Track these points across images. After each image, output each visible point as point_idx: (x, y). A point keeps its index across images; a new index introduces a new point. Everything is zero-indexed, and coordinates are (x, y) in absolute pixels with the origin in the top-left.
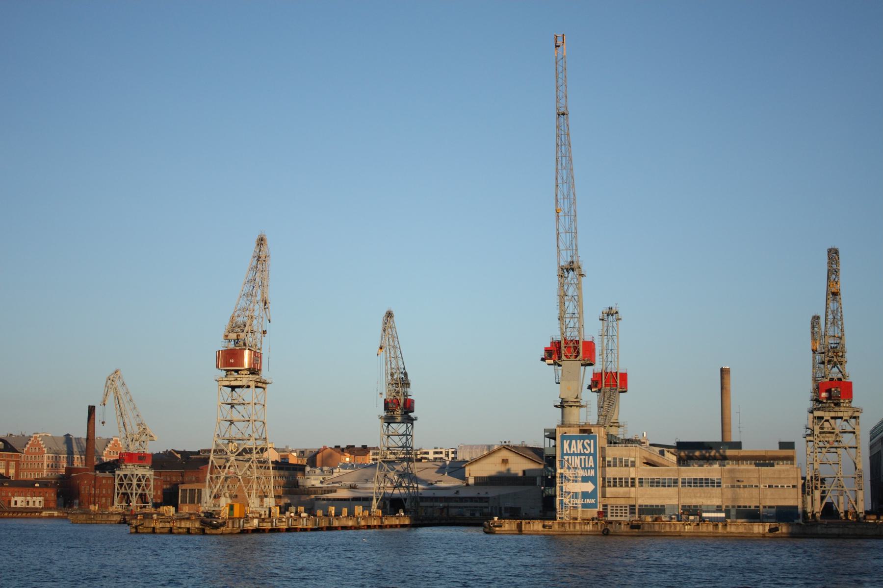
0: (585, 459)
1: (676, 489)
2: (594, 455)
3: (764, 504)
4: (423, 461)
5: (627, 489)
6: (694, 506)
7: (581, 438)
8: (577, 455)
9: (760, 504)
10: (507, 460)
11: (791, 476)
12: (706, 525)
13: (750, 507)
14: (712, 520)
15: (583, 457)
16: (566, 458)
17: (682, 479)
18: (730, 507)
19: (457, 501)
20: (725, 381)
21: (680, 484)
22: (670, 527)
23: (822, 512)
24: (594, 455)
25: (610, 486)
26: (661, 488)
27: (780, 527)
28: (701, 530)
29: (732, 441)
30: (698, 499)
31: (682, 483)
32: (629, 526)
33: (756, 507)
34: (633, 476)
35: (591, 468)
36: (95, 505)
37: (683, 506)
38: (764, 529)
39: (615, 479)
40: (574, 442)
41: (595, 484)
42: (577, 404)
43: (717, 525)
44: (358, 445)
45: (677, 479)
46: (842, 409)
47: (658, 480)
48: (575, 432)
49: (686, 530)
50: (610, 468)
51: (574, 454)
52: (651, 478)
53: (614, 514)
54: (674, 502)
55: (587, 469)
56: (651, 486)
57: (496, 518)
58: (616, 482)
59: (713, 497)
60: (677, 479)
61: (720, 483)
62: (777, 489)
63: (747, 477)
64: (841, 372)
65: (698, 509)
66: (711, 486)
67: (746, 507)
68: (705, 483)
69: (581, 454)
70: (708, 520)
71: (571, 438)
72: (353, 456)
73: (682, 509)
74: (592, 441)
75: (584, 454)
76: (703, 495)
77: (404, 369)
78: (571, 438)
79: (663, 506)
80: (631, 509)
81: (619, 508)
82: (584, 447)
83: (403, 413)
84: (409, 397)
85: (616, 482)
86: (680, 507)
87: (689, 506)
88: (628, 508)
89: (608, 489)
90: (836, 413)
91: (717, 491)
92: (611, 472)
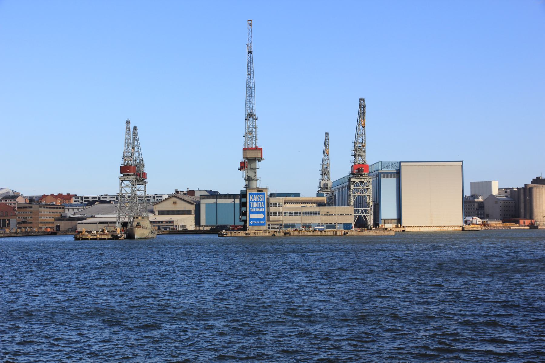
0: (260, 204)
1: (300, 216)
2: (264, 202)
3: (338, 223)
4: (112, 202)
5: (279, 216)
6: (308, 224)
7: (258, 194)
8: (256, 202)
10: (176, 202)
14: (319, 230)
15: (259, 203)
16: (251, 203)
17: (303, 212)
19: (156, 223)
20: (399, 186)
23: (374, 224)
24: (264, 202)
25: (271, 215)
30: (310, 221)
32: (284, 233)
33: (334, 224)
34: (281, 211)
35: (263, 208)
39: (274, 212)
40: (255, 196)
41: (264, 214)
42: (255, 179)
43: (322, 232)
44: (65, 193)
46: (364, 178)
48: (255, 191)
51: (255, 202)
53: (273, 228)
54: (300, 222)
55: (261, 208)
56: (289, 215)
57: (224, 231)
58: (275, 214)
62: (343, 216)
67: (330, 224)
69: (258, 201)
71: (253, 194)
72: (62, 200)
74: (263, 196)
75: (260, 201)
77: (142, 157)
78: (253, 194)
79: (294, 224)
80: (280, 226)
81: (275, 225)
82: (259, 198)
83: (324, 198)
84: (144, 172)
85: (275, 214)
86: (302, 224)
87: (306, 224)
88: (279, 225)
89: (271, 217)
91: (318, 217)
92: (272, 209)
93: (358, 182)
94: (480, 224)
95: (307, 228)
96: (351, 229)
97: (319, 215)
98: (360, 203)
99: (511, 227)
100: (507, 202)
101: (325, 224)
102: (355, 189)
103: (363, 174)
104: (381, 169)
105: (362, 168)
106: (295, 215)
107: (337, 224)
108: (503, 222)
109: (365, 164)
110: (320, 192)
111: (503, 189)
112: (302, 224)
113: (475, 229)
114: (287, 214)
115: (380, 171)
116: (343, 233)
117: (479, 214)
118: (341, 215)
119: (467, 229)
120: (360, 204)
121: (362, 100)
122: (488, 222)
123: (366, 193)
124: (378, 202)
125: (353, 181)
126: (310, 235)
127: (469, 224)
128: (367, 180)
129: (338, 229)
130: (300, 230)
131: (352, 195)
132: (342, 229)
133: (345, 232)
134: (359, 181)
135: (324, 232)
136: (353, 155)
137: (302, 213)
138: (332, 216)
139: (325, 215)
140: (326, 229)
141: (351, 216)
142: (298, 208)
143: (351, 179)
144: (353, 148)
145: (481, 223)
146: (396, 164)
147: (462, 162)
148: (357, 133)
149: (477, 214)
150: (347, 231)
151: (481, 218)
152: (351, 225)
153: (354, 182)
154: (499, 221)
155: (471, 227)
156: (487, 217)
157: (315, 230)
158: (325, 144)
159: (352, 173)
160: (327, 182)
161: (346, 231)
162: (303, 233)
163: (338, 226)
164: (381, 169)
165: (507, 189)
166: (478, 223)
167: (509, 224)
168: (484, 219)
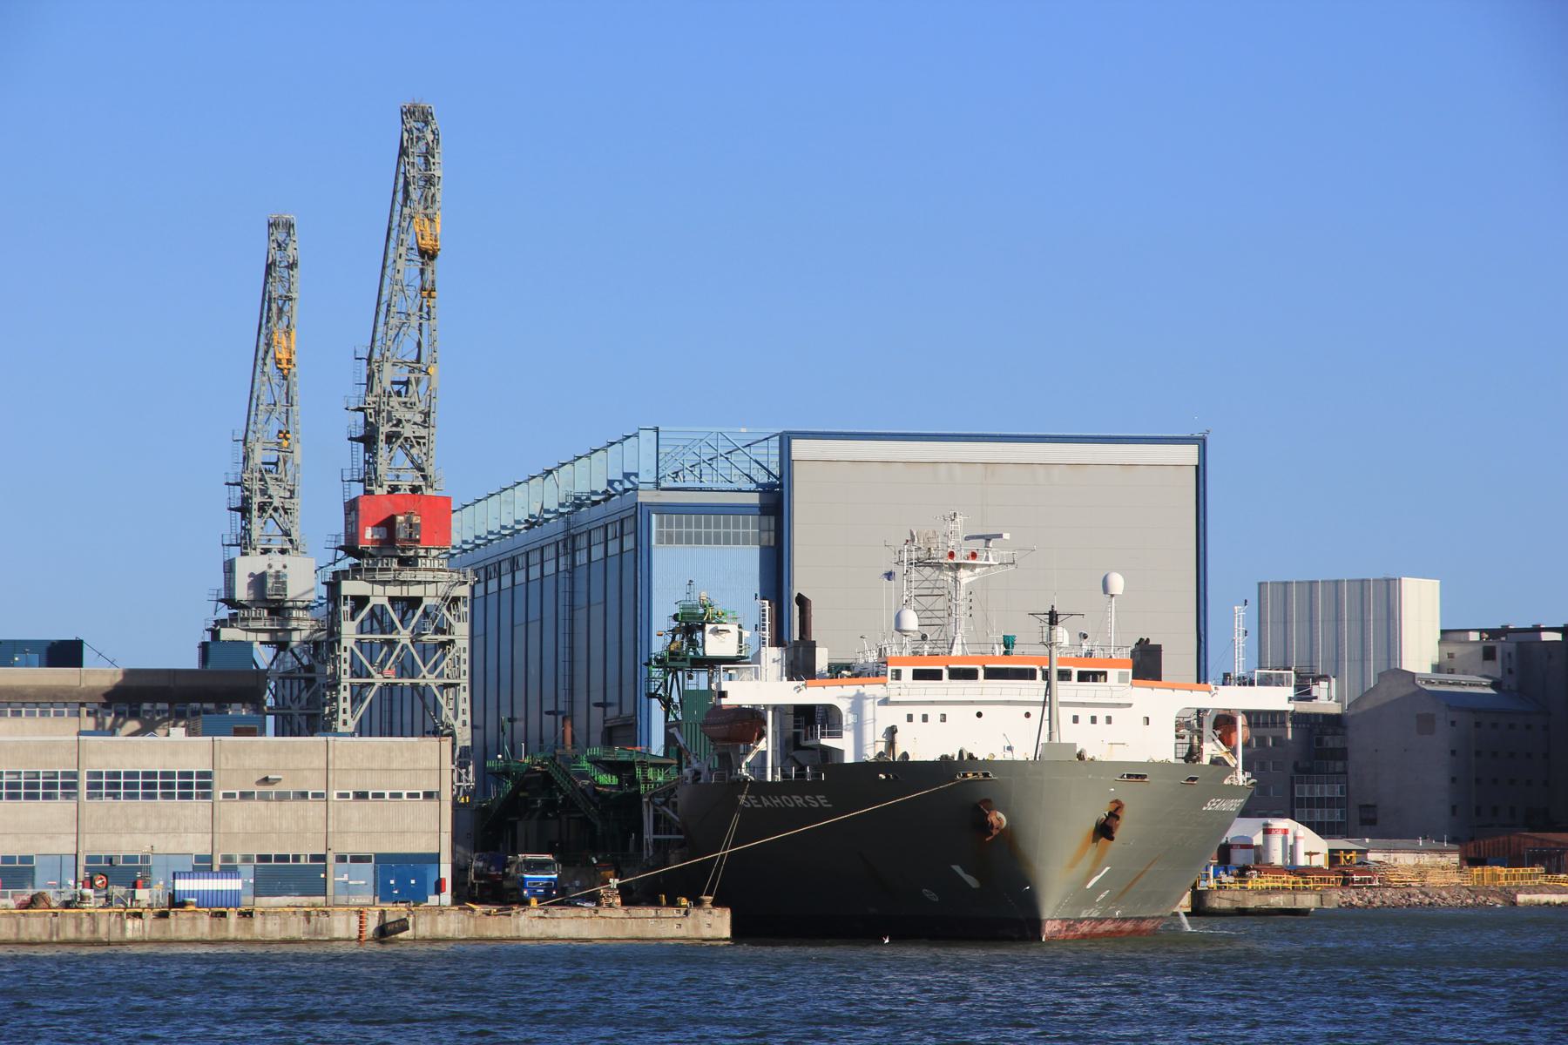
1: (70, 805)
3: (341, 851)
6: (127, 859)
9: (327, 849)
11: (423, 764)
12: (190, 915)
13: (296, 858)
14: (205, 899)
17: (91, 775)
18: (238, 860)
21: (83, 789)
22: (78, 927)
26: (23, 804)
27: (411, 920)
28: (173, 934)
29: (817, 649)
31: (90, 786)
33: (314, 858)
36: (495, 870)
37: (90, 859)
38: (264, 923)
43: (223, 915)
45: (75, 775)
47: (13, 779)
49: (129, 935)
50: (1258, 729)
52: (180, 773)
54: (66, 846)
59: (186, 831)
60: (75, 775)
61: (208, 785)
62: (378, 803)
63: (291, 766)
64: (421, 469)
65: (139, 869)
66: (64, 795)
67: (284, 858)
68: (126, 786)
70: (195, 900)
73: (87, 869)
76: (154, 824)
86: (82, 861)
87: (110, 860)
90: (405, 588)
91: (196, 809)
93: (385, 601)
94: (1318, 870)
95: (118, 891)
96: (433, 900)
97: (206, 796)
98: (549, 706)
99: (1520, 890)
100: (1494, 725)
101: (247, 859)
102: (366, 648)
103: (417, 557)
104: (657, 484)
105: (408, 520)
106: (34, 797)
107: (331, 859)
108: (1472, 861)
109: (429, 492)
110: (227, 634)
111: (1474, 636)
112: (82, 861)
113: (1279, 901)
114: (866, 674)
115: (644, 497)
116: (372, 924)
117: (1311, 803)
118: (362, 796)
119: (1226, 905)
120: (555, 713)
121: (417, 115)
122: (1372, 856)
123: (430, 672)
124: (628, 711)
125: (353, 598)
126: (138, 935)
127: (1242, 872)
128: (442, 589)
129: (342, 899)
130: (67, 905)
131: (346, 680)
132: (367, 899)
133: (390, 918)
134: (392, 600)
135: (243, 915)
136: (360, 432)
137: (84, 781)
138: (301, 804)
139: (245, 796)
140: (256, 894)
141: (434, 803)
142: (50, 747)
143: (344, 583)
144: (356, 395)
145: (1320, 861)
146: (759, 452)
147: (1202, 443)
148: (382, 307)
149: (1301, 803)
150: (402, 907)
151: (1322, 830)
152: (431, 868)
153: (360, 602)
154: (1442, 852)
155: (1258, 892)
156: (1364, 822)
157: (177, 901)
158: (267, 299)
159: (351, 549)
160: (277, 567)
161: (395, 912)
162: (86, 926)
163: (337, 876)
164: (657, 484)
165: (1494, 634)
166: (1302, 861)
167: (1502, 871)
168: (1347, 835)
